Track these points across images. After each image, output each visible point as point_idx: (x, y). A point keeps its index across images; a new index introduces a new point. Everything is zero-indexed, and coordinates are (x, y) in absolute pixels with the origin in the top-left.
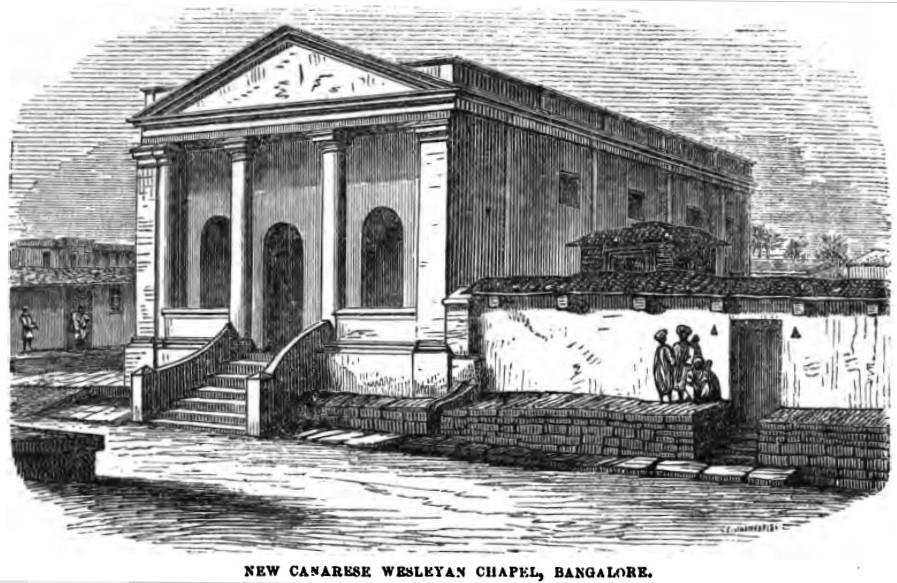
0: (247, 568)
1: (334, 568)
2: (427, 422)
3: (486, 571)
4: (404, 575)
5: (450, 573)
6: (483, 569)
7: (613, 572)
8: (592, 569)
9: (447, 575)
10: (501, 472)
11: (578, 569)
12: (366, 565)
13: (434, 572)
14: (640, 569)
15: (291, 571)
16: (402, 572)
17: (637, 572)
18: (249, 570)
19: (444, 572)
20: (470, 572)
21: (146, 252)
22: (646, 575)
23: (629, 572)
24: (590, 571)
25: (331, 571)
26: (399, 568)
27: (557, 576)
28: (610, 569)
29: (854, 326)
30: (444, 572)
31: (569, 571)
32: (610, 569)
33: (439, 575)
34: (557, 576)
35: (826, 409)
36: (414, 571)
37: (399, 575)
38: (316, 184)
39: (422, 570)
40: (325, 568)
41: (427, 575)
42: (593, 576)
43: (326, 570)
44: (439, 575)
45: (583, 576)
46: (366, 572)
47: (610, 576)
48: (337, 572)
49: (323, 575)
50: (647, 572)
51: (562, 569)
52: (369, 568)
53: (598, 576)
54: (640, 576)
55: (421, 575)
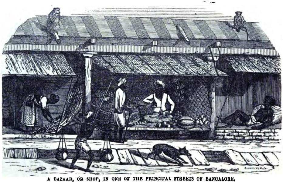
0: (83, 180)
1: (70, 178)
2: (117, 113)
3: (160, 179)
6: (159, 177)
7: (223, 179)
10: (185, 140)
12: (129, 177)
15: (124, 179)
17: (118, 179)
20: (144, 179)
22: (233, 181)
25: (69, 179)
27: (54, 180)
38: (267, 96)
43: (58, 179)
45: (214, 180)
46: (120, 179)
47: (222, 180)
49: (219, 181)
50: (234, 179)
52: (121, 178)
53: (219, 181)
54: (140, 180)
55: (185, 180)
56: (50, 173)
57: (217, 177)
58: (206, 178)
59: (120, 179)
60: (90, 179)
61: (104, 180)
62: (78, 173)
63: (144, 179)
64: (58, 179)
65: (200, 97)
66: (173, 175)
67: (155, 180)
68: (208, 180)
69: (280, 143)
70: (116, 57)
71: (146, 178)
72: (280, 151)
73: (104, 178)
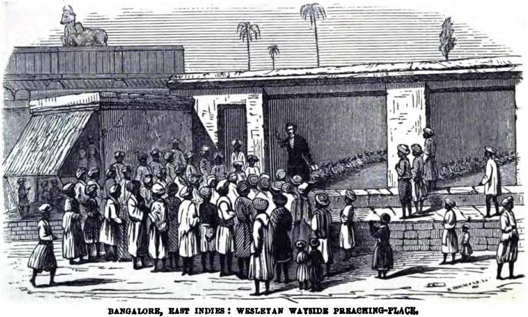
4: (249, 313)
5: (274, 312)
7: (141, 311)
8: (130, 309)
9: (273, 313)
11: (121, 309)
13: (266, 311)
14: (156, 309)
16: (250, 311)
18: (111, 311)
19: (271, 311)
20: (331, 311)
21: (111, 270)
23: (150, 311)
24: (128, 310)
25: (277, 311)
26: (246, 309)
28: (139, 309)
29: (491, 169)
30: (271, 311)
31: (117, 310)
32: (139, 309)
33: (269, 313)
34: (110, 313)
35: (386, 105)
36: (255, 310)
37: (246, 313)
39: (259, 310)
40: (134, 309)
41: (262, 313)
42: (129, 313)
44: (269, 313)
46: (326, 311)
47: (139, 313)
48: (348, 311)
50: (160, 311)
51: (113, 310)
53: (133, 313)
55: (259, 313)
56: (188, 210)
57: (130, 309)
58: (108, 310)
59: (326, 311)
60: (314, 311)
61: (196, 313)
62: (26, 276)
63: (331, 311)
64: (117, 310)
65: (489, 240)
66: (286, 305)
67: (200, 313)
68: (112, 313)
69: (174, 281)
70: (128, 101)
71: (335, 309)
72: (362, 290)
73: (196, 309)
